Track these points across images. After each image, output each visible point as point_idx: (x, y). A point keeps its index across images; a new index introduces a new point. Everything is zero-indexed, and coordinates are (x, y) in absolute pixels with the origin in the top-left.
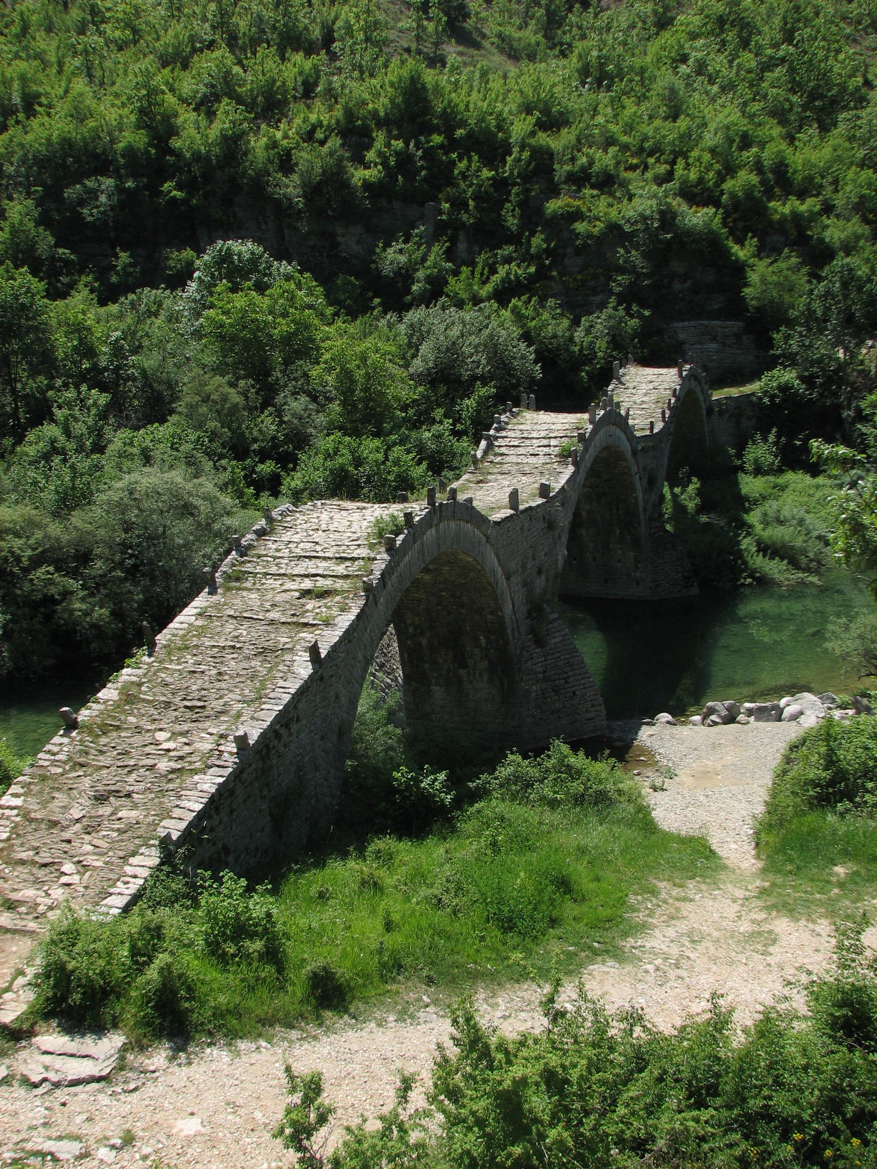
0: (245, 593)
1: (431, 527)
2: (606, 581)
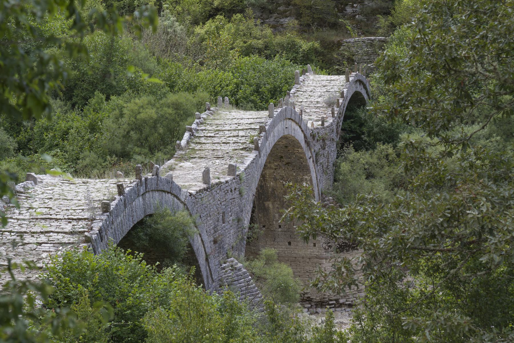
1: (139, 196)
2: (290, 243)
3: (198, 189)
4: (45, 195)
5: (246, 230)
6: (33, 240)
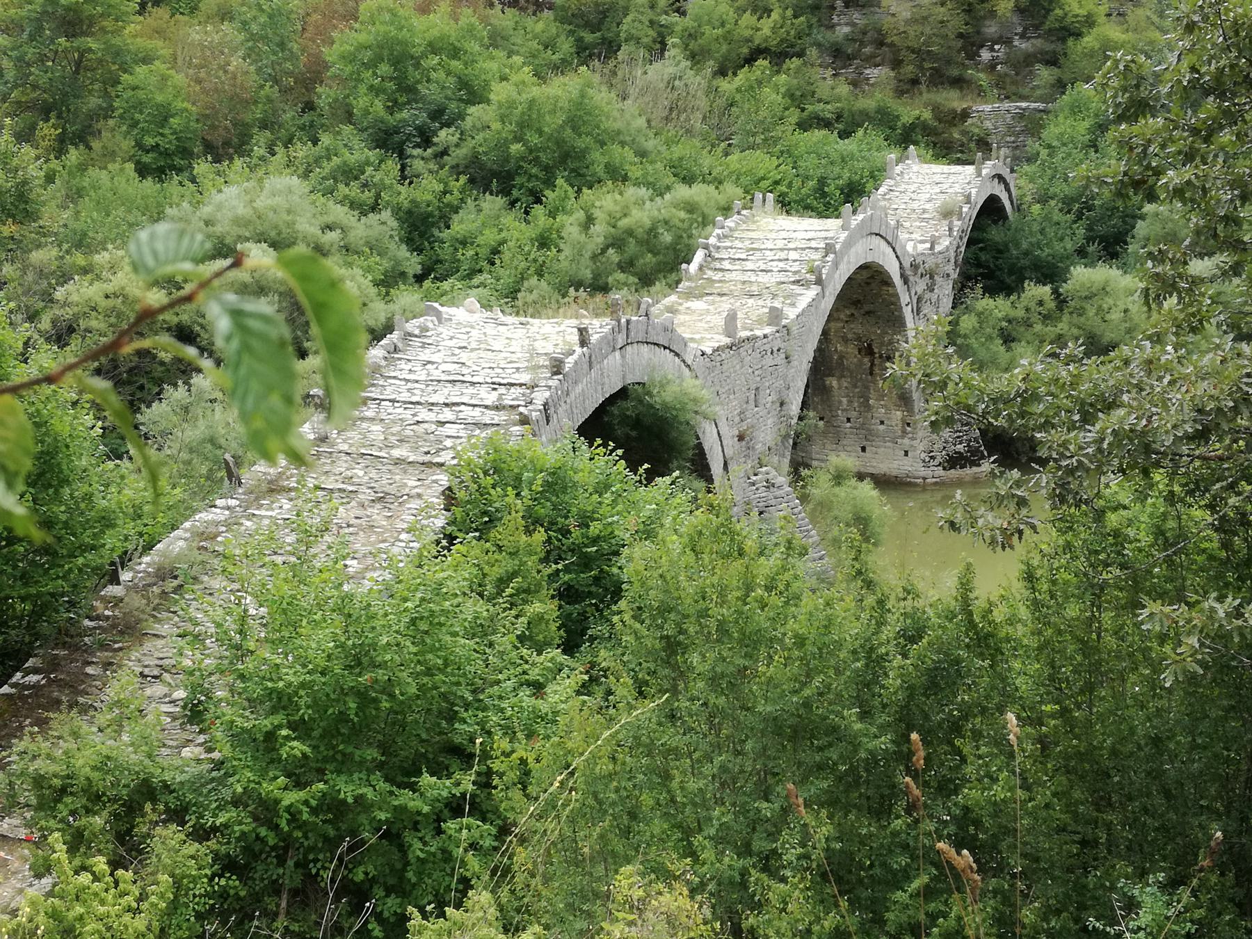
0: (365, 425)
1: (614, 350)
2: (863, 449)
3: (717, 345)
4: (455, 341)
5: (795, 420)
6: (431, 416)
